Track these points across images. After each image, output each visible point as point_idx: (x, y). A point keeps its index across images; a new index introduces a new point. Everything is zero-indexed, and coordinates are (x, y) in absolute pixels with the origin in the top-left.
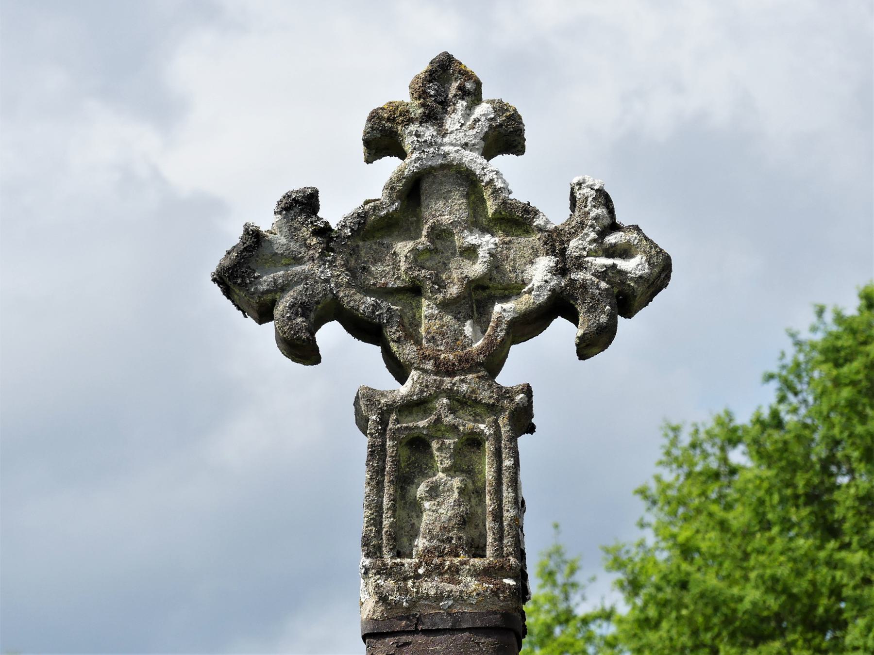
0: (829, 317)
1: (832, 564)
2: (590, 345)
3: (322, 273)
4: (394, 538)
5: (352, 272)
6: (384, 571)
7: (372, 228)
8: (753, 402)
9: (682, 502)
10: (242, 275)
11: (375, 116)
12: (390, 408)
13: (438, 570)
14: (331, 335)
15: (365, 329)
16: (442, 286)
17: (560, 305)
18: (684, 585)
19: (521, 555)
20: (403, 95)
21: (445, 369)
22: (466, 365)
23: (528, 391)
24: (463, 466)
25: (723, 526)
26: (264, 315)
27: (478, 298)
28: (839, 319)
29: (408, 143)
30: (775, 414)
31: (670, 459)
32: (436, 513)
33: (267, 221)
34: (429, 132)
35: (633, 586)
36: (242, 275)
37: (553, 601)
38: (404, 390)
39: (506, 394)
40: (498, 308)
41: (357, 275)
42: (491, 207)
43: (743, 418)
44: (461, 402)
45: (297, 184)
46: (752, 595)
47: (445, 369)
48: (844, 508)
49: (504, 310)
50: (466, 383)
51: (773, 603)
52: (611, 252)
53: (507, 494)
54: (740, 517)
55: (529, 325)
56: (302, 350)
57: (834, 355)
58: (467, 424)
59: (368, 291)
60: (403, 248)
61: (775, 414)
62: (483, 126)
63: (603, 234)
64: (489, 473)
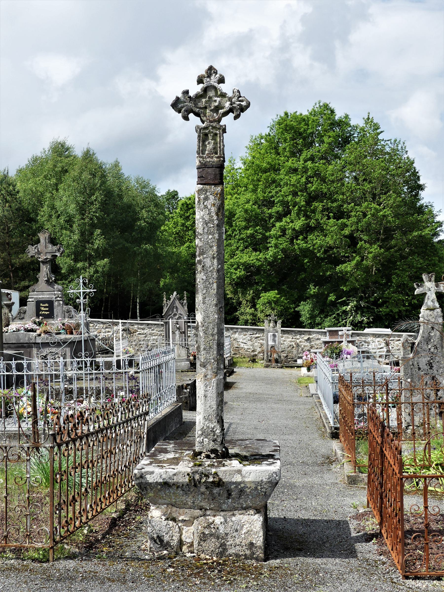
0: (279, 116)
1: (278, 160)
2: (236, 118)
3: (190, 105)
4: (202, 151)
5: (195, 104)
6: (200, 157)
7: (198, 97)
8: (266, 131)
9: (253, 149)
10: (176, 105)
11: (199, 77)
12: (201, 128)
13: (210, 157)
14: (191, 116)
15: (197, 115)
16: (210, 107)
17: (231, 110)
18: (253, 163)
19: (224, 154)
20: (204, 73)
21: (211, 122)
22: (215, 121)
23: (225, 126)
24: (214, 139)
25: (260, 153)
26: (179, 112)
27: (216, 109)
28: (281, 117)
29: (205, 81)
30: (269, 134)
31: (251, 141)
32: (209, 147)
33: (180, 95)
34: (208, 79)
35: (245, 163)
36: (176, 105)
37: (231, 166)
38: (204, 125)
39: (222, 126)
40: (220, 111)
41: (196, 105)
42: (219, 93)
43: (264, 134)
44: (214, 128)
45: (185, 89)
46: (265, 165)
47: (211, 122)
48: (280, 150)
49: (221, 111)
50: (214, 124)
51: (268, 166)
52: (240, 101)
53: (222, 144)
54: (263, 151)
55: (226, 114)
56: (186, 118)
57: (279, 123)
58: (215, 131)
59: (198, 108)
60: (204, 100)
61: (269, 134)
62: (218, 78)
63: (238, 98)
64: (218, 140)
